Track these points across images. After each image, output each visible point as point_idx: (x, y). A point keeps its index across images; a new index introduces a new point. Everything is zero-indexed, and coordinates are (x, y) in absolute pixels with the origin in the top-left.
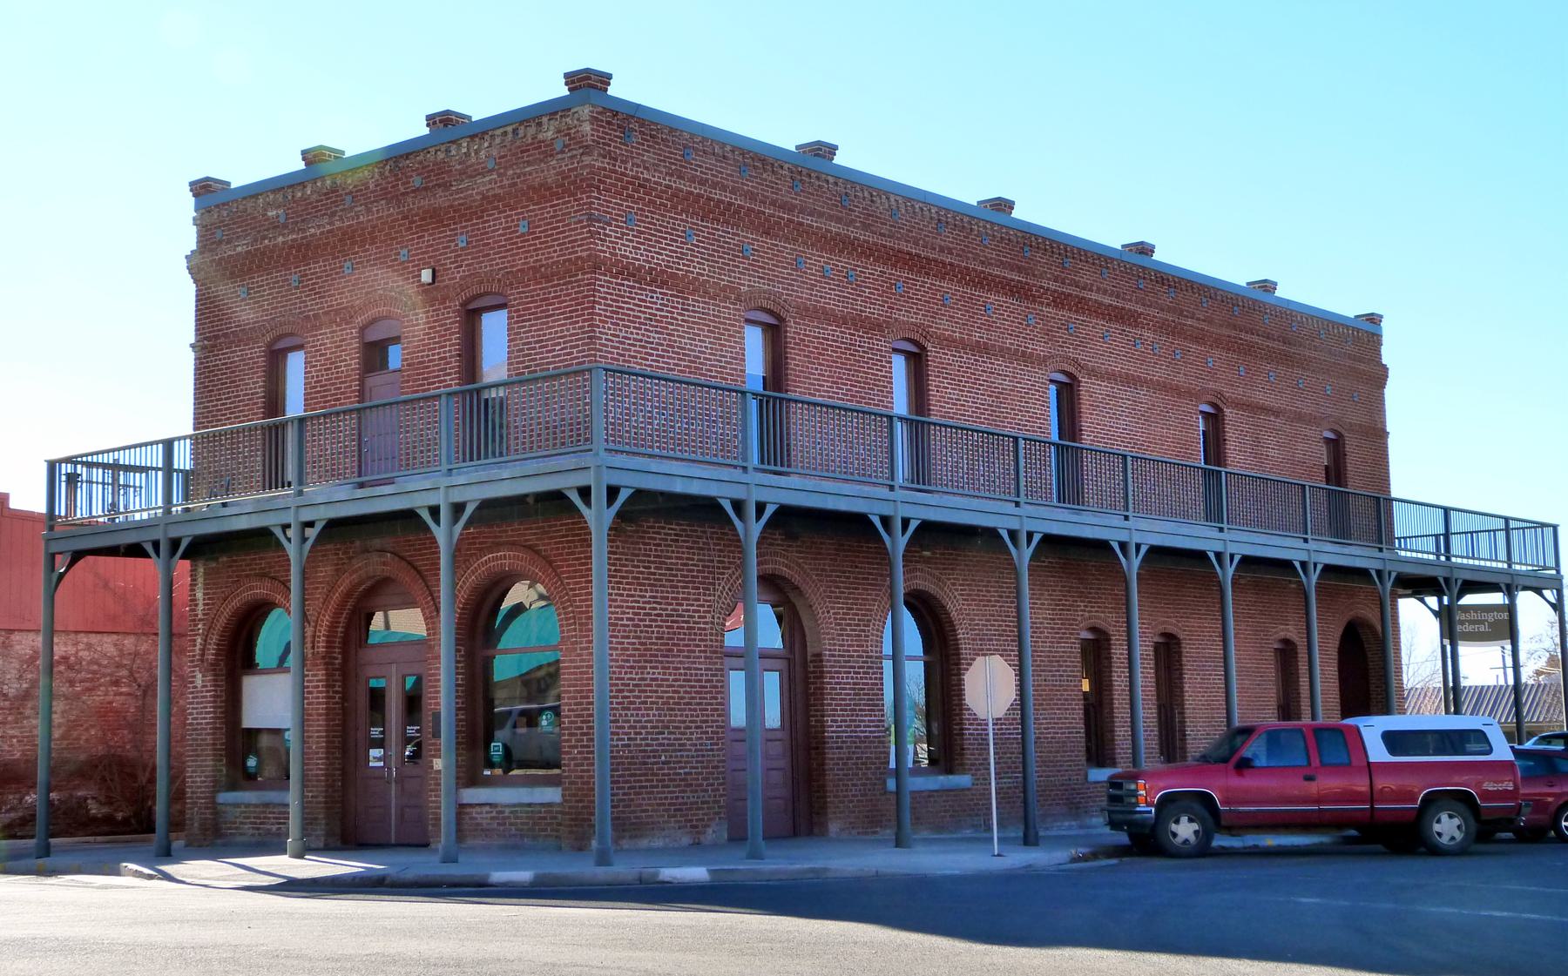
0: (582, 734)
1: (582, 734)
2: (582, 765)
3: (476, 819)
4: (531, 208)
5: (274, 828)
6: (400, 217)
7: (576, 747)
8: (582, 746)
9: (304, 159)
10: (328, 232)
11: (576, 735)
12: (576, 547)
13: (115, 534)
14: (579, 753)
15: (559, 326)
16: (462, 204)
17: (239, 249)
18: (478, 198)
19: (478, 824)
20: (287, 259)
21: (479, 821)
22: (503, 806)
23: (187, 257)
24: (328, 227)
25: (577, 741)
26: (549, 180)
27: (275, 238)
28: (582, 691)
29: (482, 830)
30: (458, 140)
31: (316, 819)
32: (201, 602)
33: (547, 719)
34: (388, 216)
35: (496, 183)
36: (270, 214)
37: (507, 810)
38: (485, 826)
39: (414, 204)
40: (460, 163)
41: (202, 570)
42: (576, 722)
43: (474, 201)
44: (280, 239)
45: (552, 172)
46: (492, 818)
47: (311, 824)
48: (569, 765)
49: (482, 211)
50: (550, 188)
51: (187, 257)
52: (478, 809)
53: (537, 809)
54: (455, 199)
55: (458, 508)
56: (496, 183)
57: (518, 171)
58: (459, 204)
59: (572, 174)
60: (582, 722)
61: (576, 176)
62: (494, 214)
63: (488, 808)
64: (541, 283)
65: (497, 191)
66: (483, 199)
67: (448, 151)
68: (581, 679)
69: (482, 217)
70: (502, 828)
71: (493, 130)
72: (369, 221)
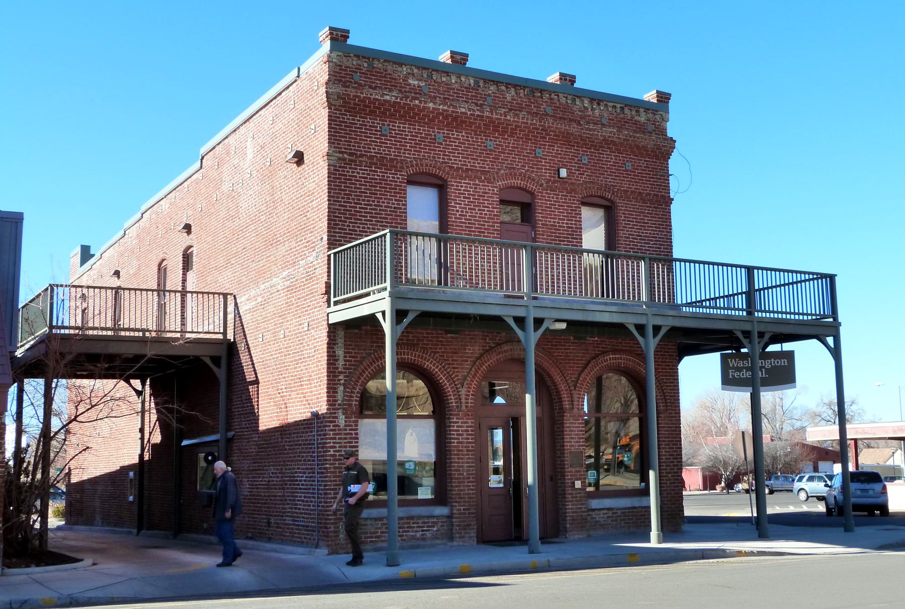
0: (674, 466)
1: (674, 466)
2: (674, 483)
3: (596, 518)
4: (632, 156)
5: (418, 535)
6: (541, 128)
7: (670, 473)
8: (674, 473)
9: (452, 57)
10: (478, 116)
11: (671, 466)
12: (666, 358)
13: (476, 304)
14: (672, 476)
15: (652, 230)
16: (589, 138)
17: (388, 98)
18: (601, 138)
19: (596, 522)
20: (432, 120)
21: (597, 519)
22: (617, 509)
23: (675, 141)
24: (478, 113)
25: (670, 469)
26: (649, 146)
27: (425, 102)
28: (673, 441)
29: (600, 525)
30: (582, 97)
31: (469, 525)
32: (341, 358)
33: (628, 457)
34: (532, 124)
35: (615, 134)
36: (411, 81)
37: (619, 512)
38: (602, 522)
39: (553, 124)
40: (580, 111)
41: (343, 333)
42: (670, 459)
43: (598, 139)
44: (431, 105)
45: (652, 142)
46: (609, 517)
47: (465, 529)
48: (666, 483)
49: (601, 147)
50: (647, 151)
51: (675, 141)
52: (597, 512)
53: (639, 510)
54: (584, 133)
55: (657, 329)
56: (615, 134)
57: (631, 134)
58: (587, 137)
59: (514, 124)
60: (674, 459)
61: (665, 150)
62: (607, 151)
63: (605, 511)
64: (639, 202)
65: (615, 139)
66: (604, 140)
67: (574, 100)
68: (672, 434)
69: (598, 150)
70: (614, 523)
71: (608, 101)
72: (514, 121)
